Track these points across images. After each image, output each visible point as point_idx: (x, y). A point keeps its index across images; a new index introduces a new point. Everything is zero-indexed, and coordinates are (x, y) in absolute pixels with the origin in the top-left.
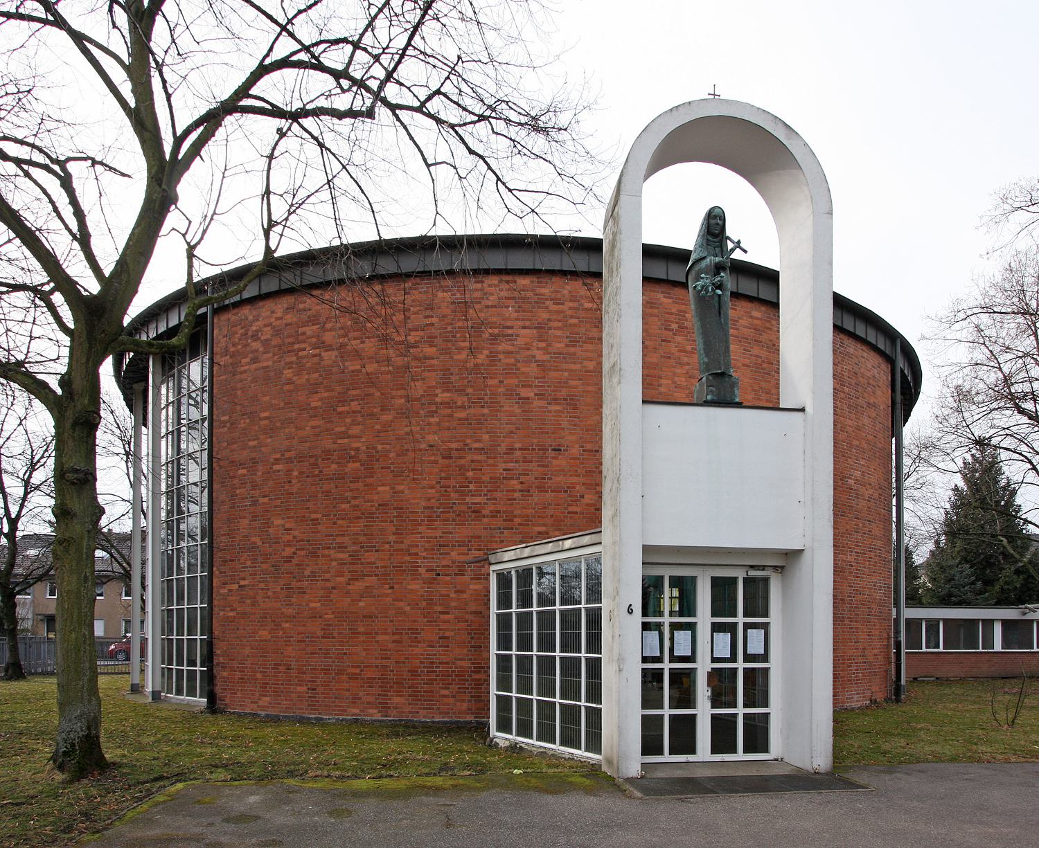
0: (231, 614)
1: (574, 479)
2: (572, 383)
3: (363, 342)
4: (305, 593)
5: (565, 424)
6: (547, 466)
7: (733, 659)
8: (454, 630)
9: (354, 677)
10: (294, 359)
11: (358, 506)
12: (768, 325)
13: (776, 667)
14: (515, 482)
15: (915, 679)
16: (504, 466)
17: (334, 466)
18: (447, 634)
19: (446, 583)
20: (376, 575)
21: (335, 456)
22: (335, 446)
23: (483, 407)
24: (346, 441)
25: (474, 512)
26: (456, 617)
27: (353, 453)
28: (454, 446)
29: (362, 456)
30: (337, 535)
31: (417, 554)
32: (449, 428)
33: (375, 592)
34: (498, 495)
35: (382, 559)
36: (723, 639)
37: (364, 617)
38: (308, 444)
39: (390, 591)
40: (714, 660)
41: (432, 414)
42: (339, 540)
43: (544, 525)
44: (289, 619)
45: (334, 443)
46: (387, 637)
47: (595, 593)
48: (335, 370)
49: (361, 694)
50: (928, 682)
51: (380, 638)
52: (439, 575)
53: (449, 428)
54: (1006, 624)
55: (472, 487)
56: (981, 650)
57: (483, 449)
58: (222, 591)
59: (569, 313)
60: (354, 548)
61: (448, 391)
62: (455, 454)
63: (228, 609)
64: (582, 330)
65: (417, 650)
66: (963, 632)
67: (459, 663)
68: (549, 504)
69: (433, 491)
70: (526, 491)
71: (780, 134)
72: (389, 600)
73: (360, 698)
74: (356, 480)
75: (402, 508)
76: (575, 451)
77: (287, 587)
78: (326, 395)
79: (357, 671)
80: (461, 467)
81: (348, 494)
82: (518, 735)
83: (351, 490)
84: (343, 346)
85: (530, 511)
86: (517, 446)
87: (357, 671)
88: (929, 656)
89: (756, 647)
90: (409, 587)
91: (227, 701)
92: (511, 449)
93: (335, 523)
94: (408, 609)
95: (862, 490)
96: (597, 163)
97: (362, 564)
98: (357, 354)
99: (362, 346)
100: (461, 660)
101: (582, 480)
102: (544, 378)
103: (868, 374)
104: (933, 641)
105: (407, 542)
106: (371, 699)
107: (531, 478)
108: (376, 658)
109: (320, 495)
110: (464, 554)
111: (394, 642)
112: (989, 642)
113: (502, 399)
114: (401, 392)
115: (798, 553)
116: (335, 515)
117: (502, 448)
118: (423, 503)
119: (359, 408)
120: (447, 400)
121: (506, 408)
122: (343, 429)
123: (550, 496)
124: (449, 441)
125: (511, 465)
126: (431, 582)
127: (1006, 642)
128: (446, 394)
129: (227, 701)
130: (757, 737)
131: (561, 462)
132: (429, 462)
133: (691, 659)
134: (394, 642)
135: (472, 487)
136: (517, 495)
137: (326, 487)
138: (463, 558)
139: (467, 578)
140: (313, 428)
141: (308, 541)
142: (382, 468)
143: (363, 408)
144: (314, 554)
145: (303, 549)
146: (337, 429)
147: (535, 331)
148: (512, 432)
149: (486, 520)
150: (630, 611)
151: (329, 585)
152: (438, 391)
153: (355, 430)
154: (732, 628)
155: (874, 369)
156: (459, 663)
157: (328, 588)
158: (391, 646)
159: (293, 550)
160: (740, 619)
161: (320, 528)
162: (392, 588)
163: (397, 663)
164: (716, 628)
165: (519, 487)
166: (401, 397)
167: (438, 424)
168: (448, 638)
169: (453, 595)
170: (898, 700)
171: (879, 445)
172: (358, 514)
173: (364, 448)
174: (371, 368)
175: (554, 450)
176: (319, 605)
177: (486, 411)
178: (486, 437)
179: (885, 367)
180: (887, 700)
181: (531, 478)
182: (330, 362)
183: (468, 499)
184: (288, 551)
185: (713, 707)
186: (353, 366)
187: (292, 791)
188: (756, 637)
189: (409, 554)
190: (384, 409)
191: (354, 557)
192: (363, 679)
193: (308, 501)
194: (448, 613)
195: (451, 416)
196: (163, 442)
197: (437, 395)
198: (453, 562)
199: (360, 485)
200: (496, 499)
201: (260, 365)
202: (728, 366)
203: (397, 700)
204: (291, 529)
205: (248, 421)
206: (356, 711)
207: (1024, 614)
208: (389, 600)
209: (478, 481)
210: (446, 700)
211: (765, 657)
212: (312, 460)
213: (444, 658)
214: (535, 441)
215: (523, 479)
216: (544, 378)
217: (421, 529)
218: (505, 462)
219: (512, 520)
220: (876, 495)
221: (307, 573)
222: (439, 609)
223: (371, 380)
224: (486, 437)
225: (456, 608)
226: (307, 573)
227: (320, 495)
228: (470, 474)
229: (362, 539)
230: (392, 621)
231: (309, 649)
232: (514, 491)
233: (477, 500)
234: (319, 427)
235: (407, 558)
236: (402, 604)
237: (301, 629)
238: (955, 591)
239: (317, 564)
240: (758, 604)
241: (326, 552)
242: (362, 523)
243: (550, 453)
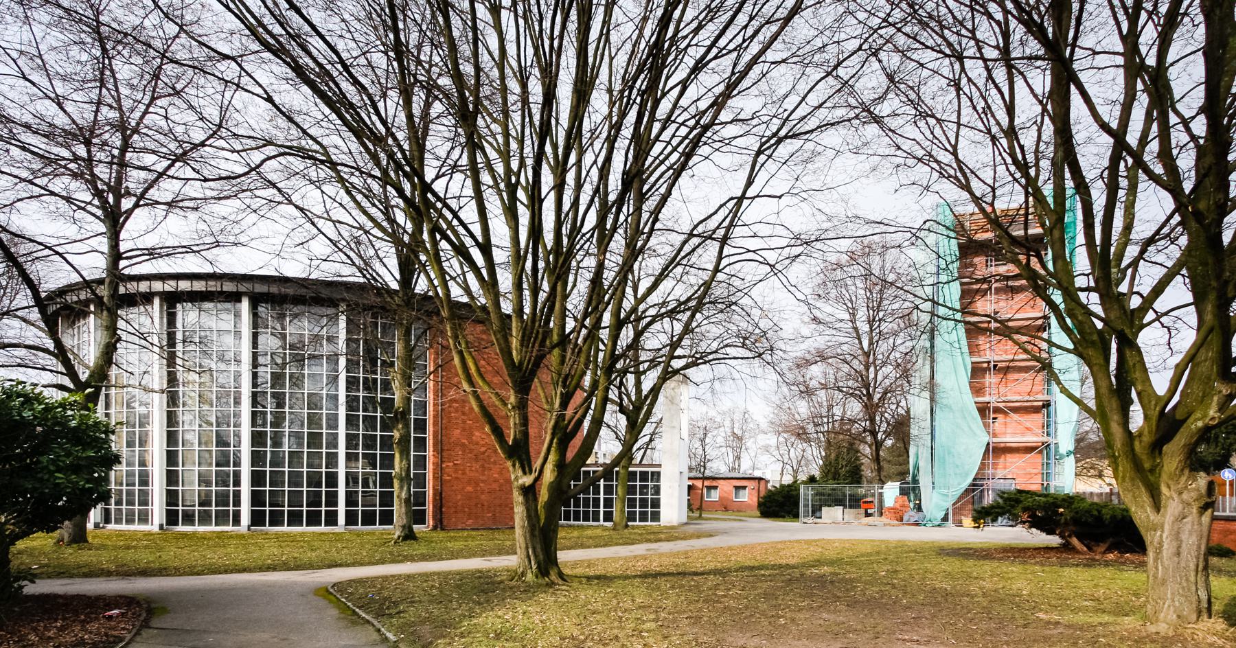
44: (483, 481)
77: (483, 466)
96: (881, 314)
184: (483, 449)
187: (1094, 560)
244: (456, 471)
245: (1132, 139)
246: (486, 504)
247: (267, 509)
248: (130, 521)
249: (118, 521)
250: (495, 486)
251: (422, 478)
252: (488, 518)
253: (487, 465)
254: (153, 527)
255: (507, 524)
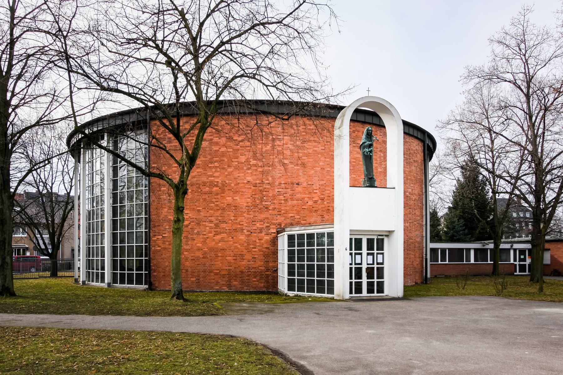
0: (159, 248)
1: (305, 196)
2: (303, 158)
3: (219, 139)
4: (194, 240)
5: (301, 174)
6: (294, 190)
7: (373, 264)
8: (258, 255)
9: (216, 274)
10: (189, 143)
11: (218, 205)
12: (376, 133)
13: (386, 266)
14: (282, 196)
15: (436, 276)
16: (278, 190)
17: (207, 188)
18: (255, 256)
19: (255, 236)
20: (226, 233)
21: (208, 184)
22: (208, 180)
23: (269, 167)
24: (213, 178)
25: (266, 208)
26: (259, 250)
27: (216, 183)
28: (258, 182)
29: (220, 185)
30: (209, 217)
31: (243, 225)
32: (256, 175)
33: (226, 240)
34: (275, 201)
35: (228, 227)
36: (370, 257)
37: (221, 250)
38: (196, 179)
39: (232, 239)
40: (368, 264)
41: (249, 169)
42: (210, 218)
43: (292, 213)
45: (207, 179)
46: (230, 258)
47: (331, 243)
48: (207, 149)
49: (220, 281)
50: (441, 277)
51: (228, 258)
52: (252, 233)
53: (256, 175)
54: (476, 250)
55: (265, 198)
56: (465, 263)
57: (269, 183)
58: (153, 239)
59: (302, 130)
60: (217, 222)
61: (255, 160)
62: (258, 185)
63: (157, 246)
64: (307, 137)
65: (244, 263)
66: (457, 254)
67: (260, 268)
68: (295, 205)
69: (249, 199)
70: (286, 200)
71: (388, 106)
72: (232, 243)
73: (219, 283)
74: (217, 194)
75: (236, 206)
76: (305, 184)
78: (204, 159)
79: (218, 271)
80: (261, 191)
81: (214, 200)
82: (297, 291)
83: (215, 198)
84: (211, 140)
85: (287, 208)
86: (283, 182)
87: (218, 271)
88: (442, 266)
89: (380, 260)
90: (240, 238)
91: (157, 285)
92: (280, 184)
93: (208, 212)
94: (239, 246)
95: (412, 197)
97: (220, 228)
98: (217, 144)
99: (219, 140)
100: (261, 266)
101: (307, 196)
102: (292, 156)
103: (414, 149)
104: (443, 259)
105: (239, 220)
106: (224, 283)
107: (288, 195)
108: (226, 266)
109: (201, 200)
110: (262, 225)
111: (234, 260)
112: (468, 259)
113: (277, 164)
114: (236, 160)
115: (393, 231)
116: (208, 208)
117: (277, 183)
118: (245, 204)
119: (218, 165)
120: (255, 164)
121: (279, 167)
122: (211, 174)
123: (295, 202)
124: (256, 180)
125: (280, 190)
126: (248, 236)
127: (476, 260)
128: (254, 161)
129: (157, 285)
130: (381, 289)
131: (299, 189)
132: (248, 188)
133: (361, 264)
134: (234, 260)
135: (265, 198)
136: (283, 202)
137: (203, 197)
138: (261, 226)
139: (263, 234)
140: (198, 172)
141: (196, 219)
142: (228, 190)
143: (220, 165)
144: (198, 224)
145: (193, 222)
146: (209, 174)
147: (289, 137)
148: (280, 177)
149: (270, 211)
150: (346, 250)
151: (205, 236)
152: (251, 160)
153: (217, 174)
154: (373, 254)
155: (416, 146)
156: (260, 268)
157: (204, 238)
158: (232, 261)
159: (189, 222)
160: (375, 251)
161: (201, 213)
162: (232, 238)
163: (235, 268)
164: (368, 254)
165: (283, 198)
166: (236, 162)
167: (251, 173)
168: (256, 258)
169: (257, 241)
170: (426, 283)
171: (419, 177)
172: (218, 208)
173: (220, 182)
174: (223, 149)
175: (297, 184)
176: (201, 245)
177: (270, 168)
178: (270, 179)
179: (421, 144)
180: (422, 283)
181: (288, 195)
182: (205, 146)
183: (264, 203)
185: (367, 279)
186: (215, 148)
188: (380, 257)
189: (240, 225)
190: (229, 166)
191: (217, 225)
192: (220, 275)
193: (196, 202)
194: (255, 248)
195: (256, 170)
196: (87, 165)
197: (251, 162)
198: (258, 228)
199: (219, 196)
200: (274, 203)
201: (172, 145)
202: (373, 175)
203: (235, 283)
204: (188, 214)
205: (166, 167)
206: (218, 288)
207: (484, 246)
208: (232, 243)
209: (267, 196)
210: (255, 283)
211: (382, 264)
212: (197, 186)
213: (255, 266)
214: (289, 180)
215: (285, 195)
216: (292, 156)
217: (244, 215)
218: (278, 189)
219: (281, 212)
220: (417, 198)
221: (195, 231)
222: (252, 246)
223: (223, 154)
224: (270, 179)
225: (259, 246)
226: (195, 231)
227: (201, 200)
228: (264, 193)
229: (220, 218)
230: (233, 251)
231: (196, 263)
232: (282, 200)
233: (267, 203)
234: (201, 172)
235: (239, 226)
236: (236, 245)
237: (193, 255)
238: (455, 234)
239: (200, 228)
240: (381, 247)
241: (204, 223)
242: (220, 212)
243: (295, 185)
244: (164, 243)
245: (41, 53)
246: (189, 269)
247: (135, 272)
248: (130, 282)
249: (122, 282)
250: (199, 254)
251: (137, 247)
252: (192, 282)
253: (189, 236)
254: (104, 285)
255: (212, 288)
